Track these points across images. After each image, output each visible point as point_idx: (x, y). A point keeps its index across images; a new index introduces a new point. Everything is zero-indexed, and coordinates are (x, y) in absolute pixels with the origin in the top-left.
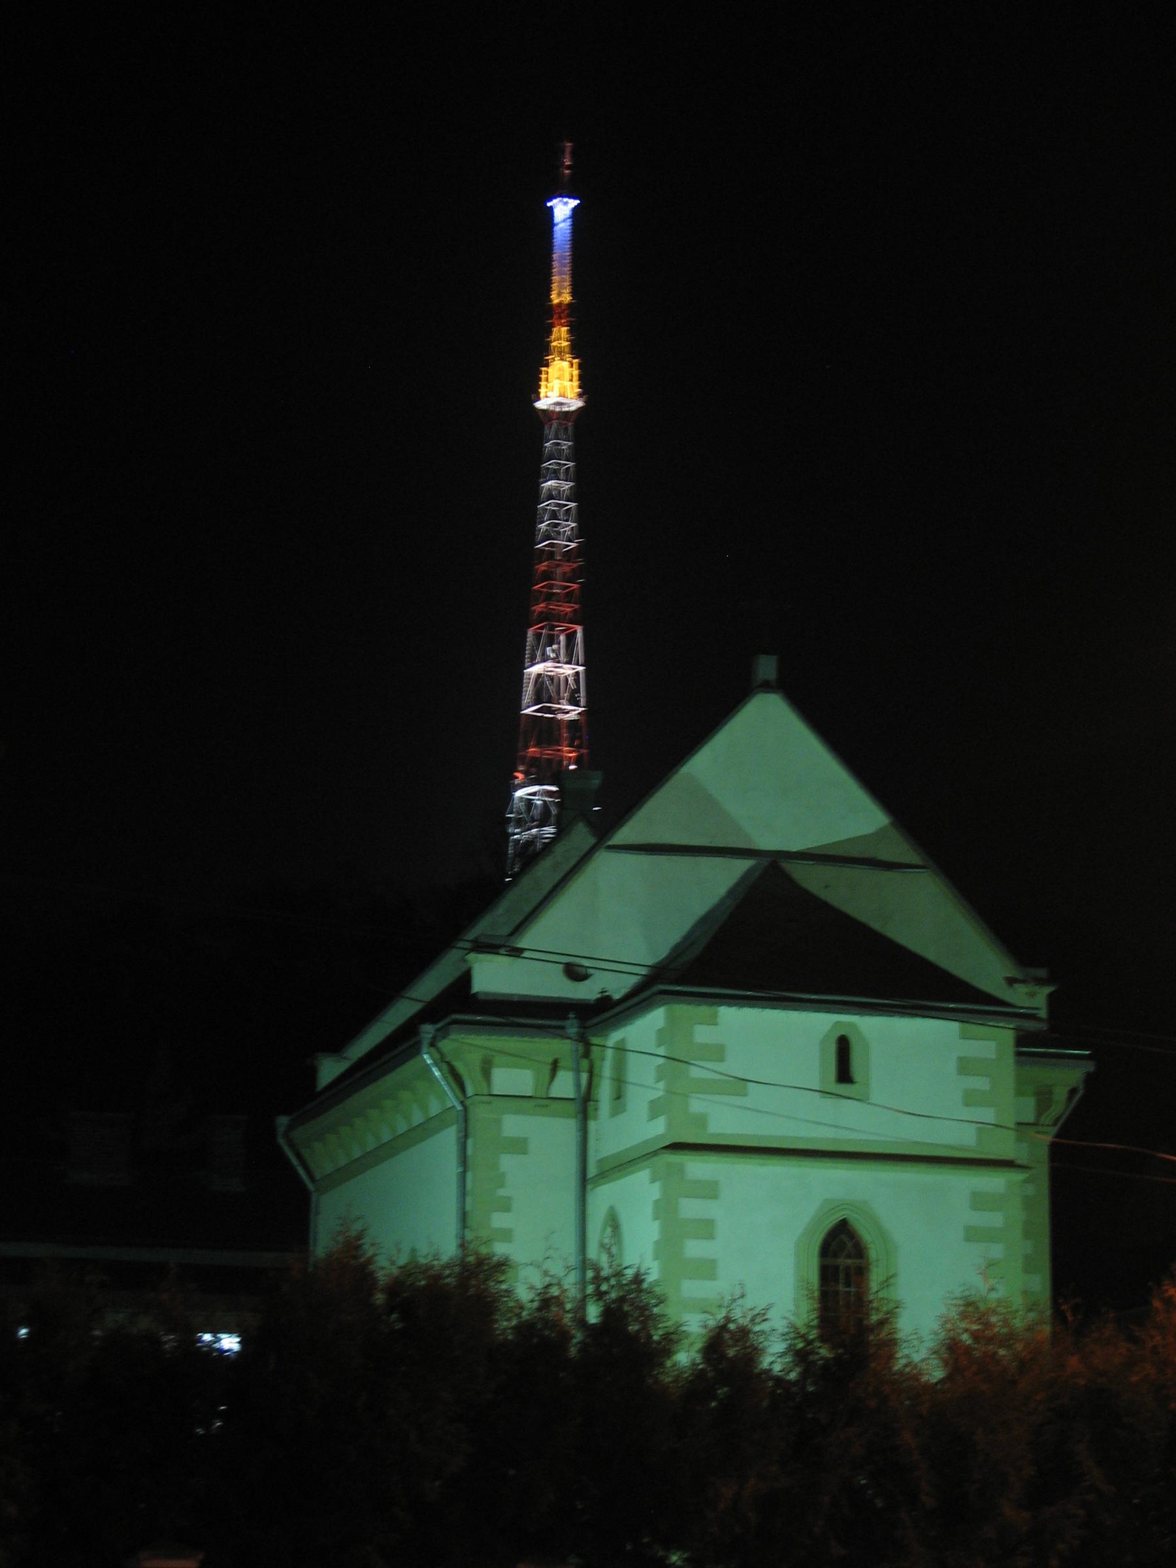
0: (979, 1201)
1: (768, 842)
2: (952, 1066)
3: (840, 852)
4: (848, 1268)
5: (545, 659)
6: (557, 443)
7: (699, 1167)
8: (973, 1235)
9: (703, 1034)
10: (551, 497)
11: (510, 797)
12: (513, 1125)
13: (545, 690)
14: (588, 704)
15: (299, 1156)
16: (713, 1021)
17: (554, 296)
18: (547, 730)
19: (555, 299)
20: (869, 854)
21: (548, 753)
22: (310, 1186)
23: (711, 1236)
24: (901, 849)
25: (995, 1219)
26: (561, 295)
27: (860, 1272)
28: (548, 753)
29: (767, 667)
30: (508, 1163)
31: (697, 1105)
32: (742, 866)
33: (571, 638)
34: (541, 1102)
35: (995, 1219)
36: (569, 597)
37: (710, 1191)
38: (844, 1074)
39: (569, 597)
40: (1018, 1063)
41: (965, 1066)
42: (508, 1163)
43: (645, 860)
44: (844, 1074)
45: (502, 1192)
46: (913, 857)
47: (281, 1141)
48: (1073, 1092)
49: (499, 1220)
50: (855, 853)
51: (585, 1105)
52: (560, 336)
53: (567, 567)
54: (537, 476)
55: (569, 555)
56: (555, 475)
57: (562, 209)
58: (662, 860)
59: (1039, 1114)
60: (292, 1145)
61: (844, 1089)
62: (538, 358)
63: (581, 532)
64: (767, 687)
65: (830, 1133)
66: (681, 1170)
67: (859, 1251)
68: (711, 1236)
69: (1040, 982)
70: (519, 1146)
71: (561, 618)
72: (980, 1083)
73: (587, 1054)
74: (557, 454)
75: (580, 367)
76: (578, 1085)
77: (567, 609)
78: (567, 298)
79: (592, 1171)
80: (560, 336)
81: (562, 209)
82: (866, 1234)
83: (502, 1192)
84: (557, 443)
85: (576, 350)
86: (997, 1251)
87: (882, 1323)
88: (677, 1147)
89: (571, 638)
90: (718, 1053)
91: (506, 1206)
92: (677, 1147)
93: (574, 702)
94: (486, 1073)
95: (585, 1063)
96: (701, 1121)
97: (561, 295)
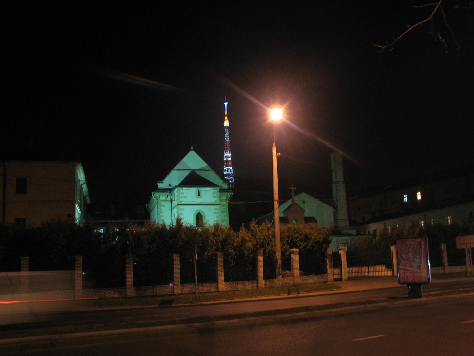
0: (215, 209)
1: (193, 168)
2: (212, 193)
3: (201, 169)
4: (200, 218)
5: (226, 153)
6: (227, 130)
7: (181, 207)
8: (215, 213)
9: (181, 191)
10: (226, 135)
11: (224, 169)
12: (163, 203)
13: (227, 157)
14: (231, 158)
15: (149, 209)
16: (183, 189)
17: (225, 113)
18: (227, 161)
19: (225, 114)
20: (205, 169)
21: (227, 164)
22: (150, 212)
23: (183, 215)
24: (209, 168)
25: (217, 211)
26: (226, 113)
27: (201, 219)
28: (227, 164)
29: (192, 148)
30: (162, 208)
31: (181, 199)
32: (189, 172)
33: (229, 151)
34: (166, 200)
35: (217, 211)
36: (229, 146)
37: (182, 210)
38: (199, 195)
39: (229, 146)
40: (220, 192)
41: (213, 193)
42: (162, 208)
43: (177, 171)
44: (199, 195)
45: (162, 211)
46: (211, 169)
47: (146, 207)
48: (231, 196)
49: (162, 214)
50: (203, 169)
51: (171, 201)
52: (226, 118)
53: (228, 143)
54: (224, 134)
55: (228, 142)
56: (227, 133)
57: (226, 104)
58: (180, 171)
59: (226, 199)
60: (148, 207)
61: (199, 197)
62: (224, 120)
63: (230, 139)
64: (192, 150)
65: (187, 202)
66: (179, 207)
67: (201, 216)
68: (183, 215)
69: (226, 183)
70: (164, 206)
71: (228, 149)
72: (215, 195)
73: (171, 194)
74: (227, 131)
75: (229, 121)
76: (170, 198)
77: (229, 148)
78: (227, 113)
79: (172, 208)
80: (226, 118)
81: (226, 104)
82: (202, 214)
83: (162, 211)
84: (227, 130)
85: (228, 119)
86: (218, 215)
87: (203, 224)
88: (179, 205)
89: (229, 151)
90: (183, 193)
91: (162, 213)
92: (179, 205)
93: (230, 158)
94: (160, 198)
95: (171, 196)
96: (181, 201)
97: (226, 113)
